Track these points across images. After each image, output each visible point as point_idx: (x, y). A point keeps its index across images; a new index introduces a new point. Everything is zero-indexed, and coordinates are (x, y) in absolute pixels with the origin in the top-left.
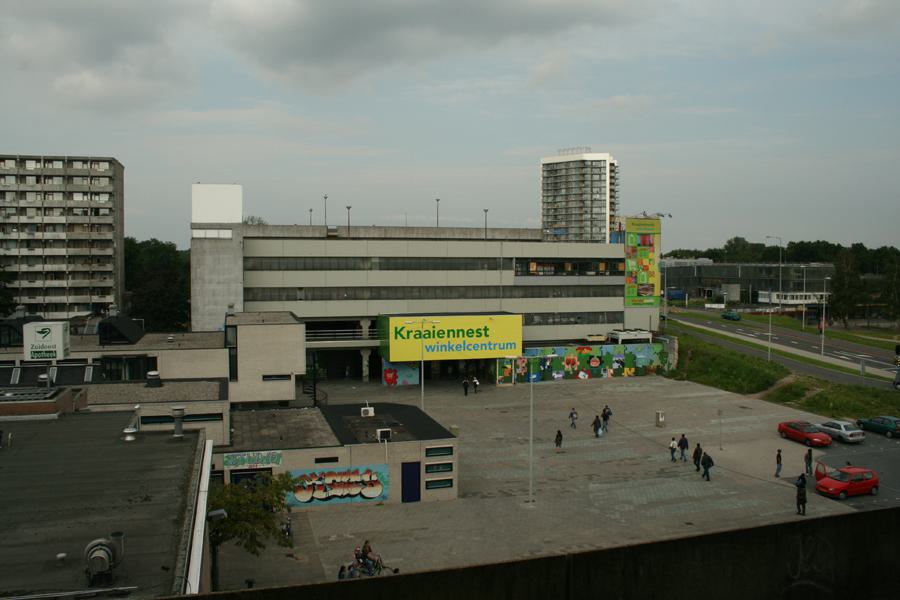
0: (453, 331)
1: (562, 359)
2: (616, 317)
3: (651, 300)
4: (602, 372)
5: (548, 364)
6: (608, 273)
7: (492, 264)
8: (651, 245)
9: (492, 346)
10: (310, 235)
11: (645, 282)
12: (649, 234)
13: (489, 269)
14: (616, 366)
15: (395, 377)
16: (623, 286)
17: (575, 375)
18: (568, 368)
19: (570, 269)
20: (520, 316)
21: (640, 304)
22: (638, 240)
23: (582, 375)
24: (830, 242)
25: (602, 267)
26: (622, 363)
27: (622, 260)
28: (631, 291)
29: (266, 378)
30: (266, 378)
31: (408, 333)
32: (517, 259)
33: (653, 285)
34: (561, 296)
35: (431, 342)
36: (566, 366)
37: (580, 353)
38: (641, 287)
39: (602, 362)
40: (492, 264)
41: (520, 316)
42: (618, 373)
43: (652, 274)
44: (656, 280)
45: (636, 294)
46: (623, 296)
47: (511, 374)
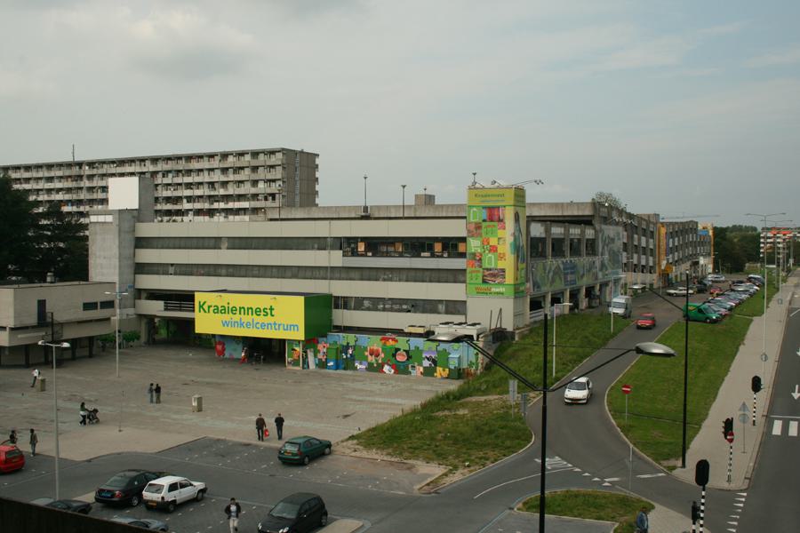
0: (244, 308)
1: (366, 349)
2: (456, 307)
3: (502, 289)
4: (410, 369)
5: (350, 352)
6: (445, 255)
7: (320, 243)
8: (500, 220)
9: (277, 327)
10: (444, 215)
11: (493, 266)
12: (498, 207)
13: (319, 249)
14: (426, 363)
15: (224, 349)
16: (465, 270)
17: (380, 368)
18: (371, 359)
19: (400, 250)
20: (303, 298)
21: (487, 293)
22: (484, 214)
23: (386, 368)
25: (438, 247)
26: (434, 362)
27: (463, 240)
28: (474, 277)
31: (209, 307)
33: (503, 271)
34: (391, 280)
35: (227, 317)
36: (370, 357)
37: (385, 344)
38: (487, 273)
39: (409, 357)
40: (320, 243)
41: (303, 298)
42: (429, 372)
43: (502, 257)
44: (508, 263)
45: (480, 280)
46: (464, 282)
47: (299, 356)
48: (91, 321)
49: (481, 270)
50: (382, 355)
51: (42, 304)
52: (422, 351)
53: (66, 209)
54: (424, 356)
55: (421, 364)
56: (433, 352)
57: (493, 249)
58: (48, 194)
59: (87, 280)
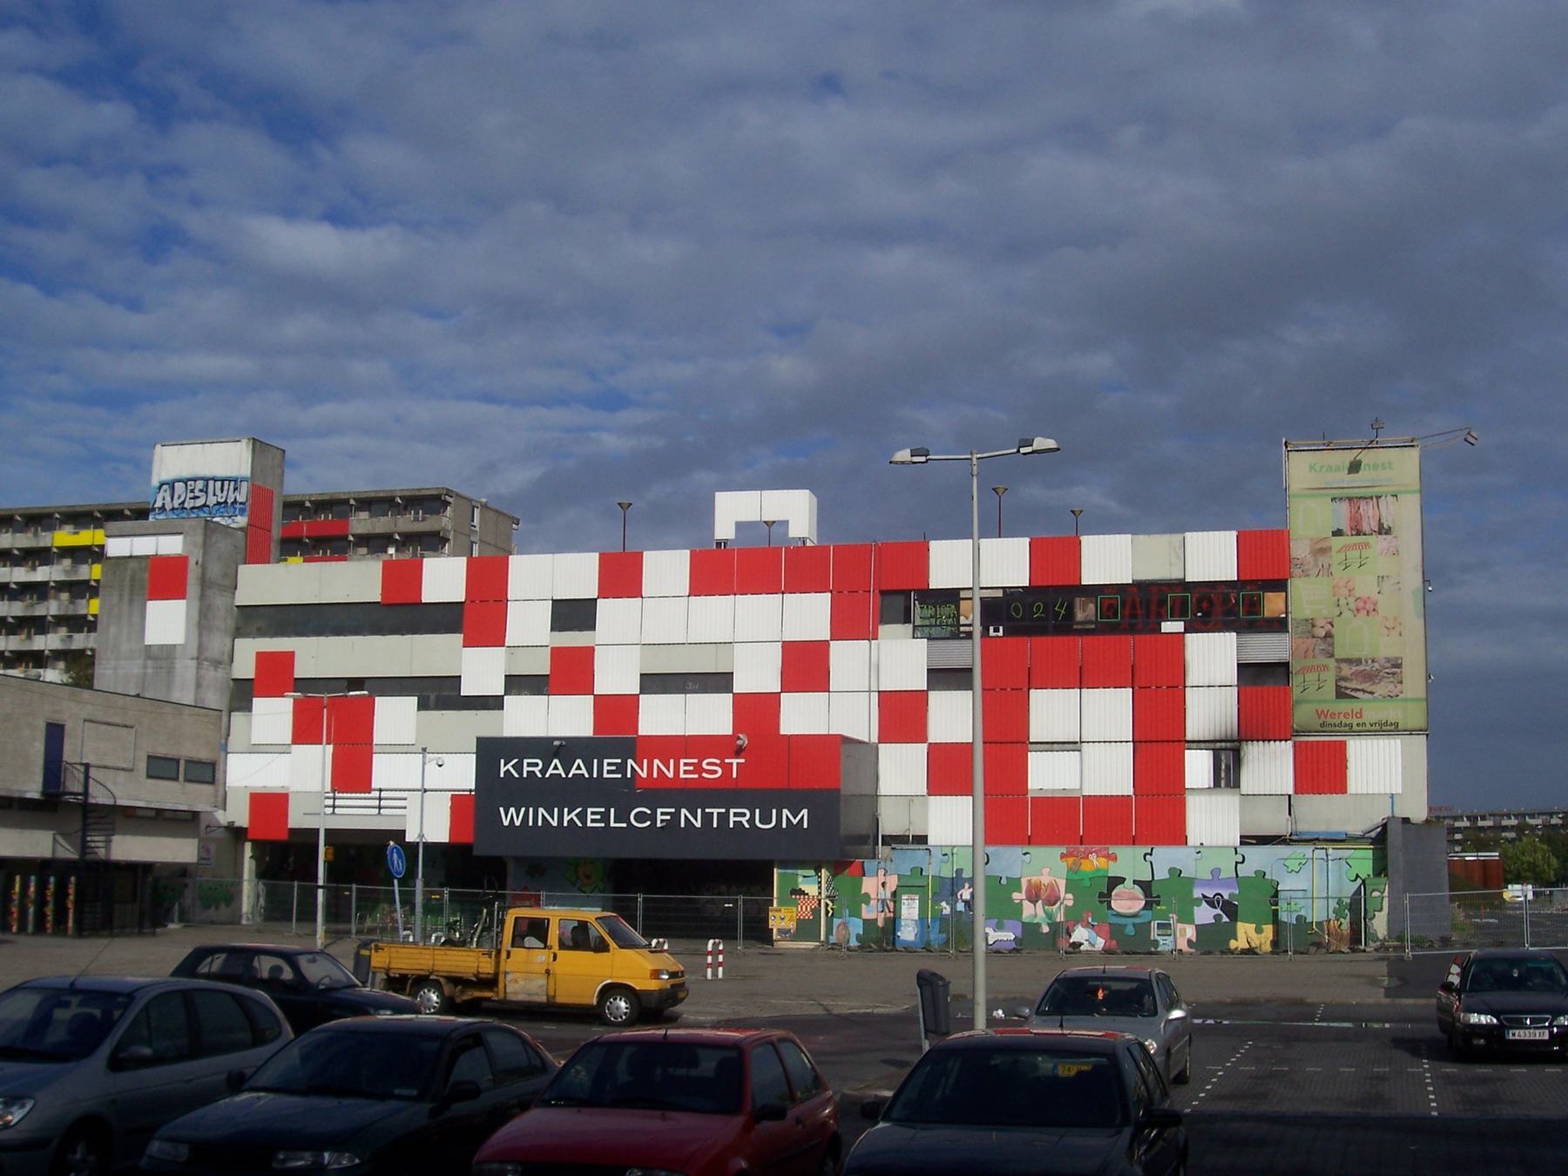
1: (1015, 884)
14: (1205, 914)
16: (1286, 665)
18: (1032, 912)
24: (450, 804)
26: (1230, 909)
29: (305, 814)
30: (305, 814)
36: (1028, 907)
45: (1330, 690)
47: (816, 912)
48: (973, 724)
49: (1332, 663)
50: (1069, 900)
51: (55, 734)
54: (1197, 893)
55: (1187, 918)
56: (1226, 883)
57: (1366, 608)
59: (464, 646)
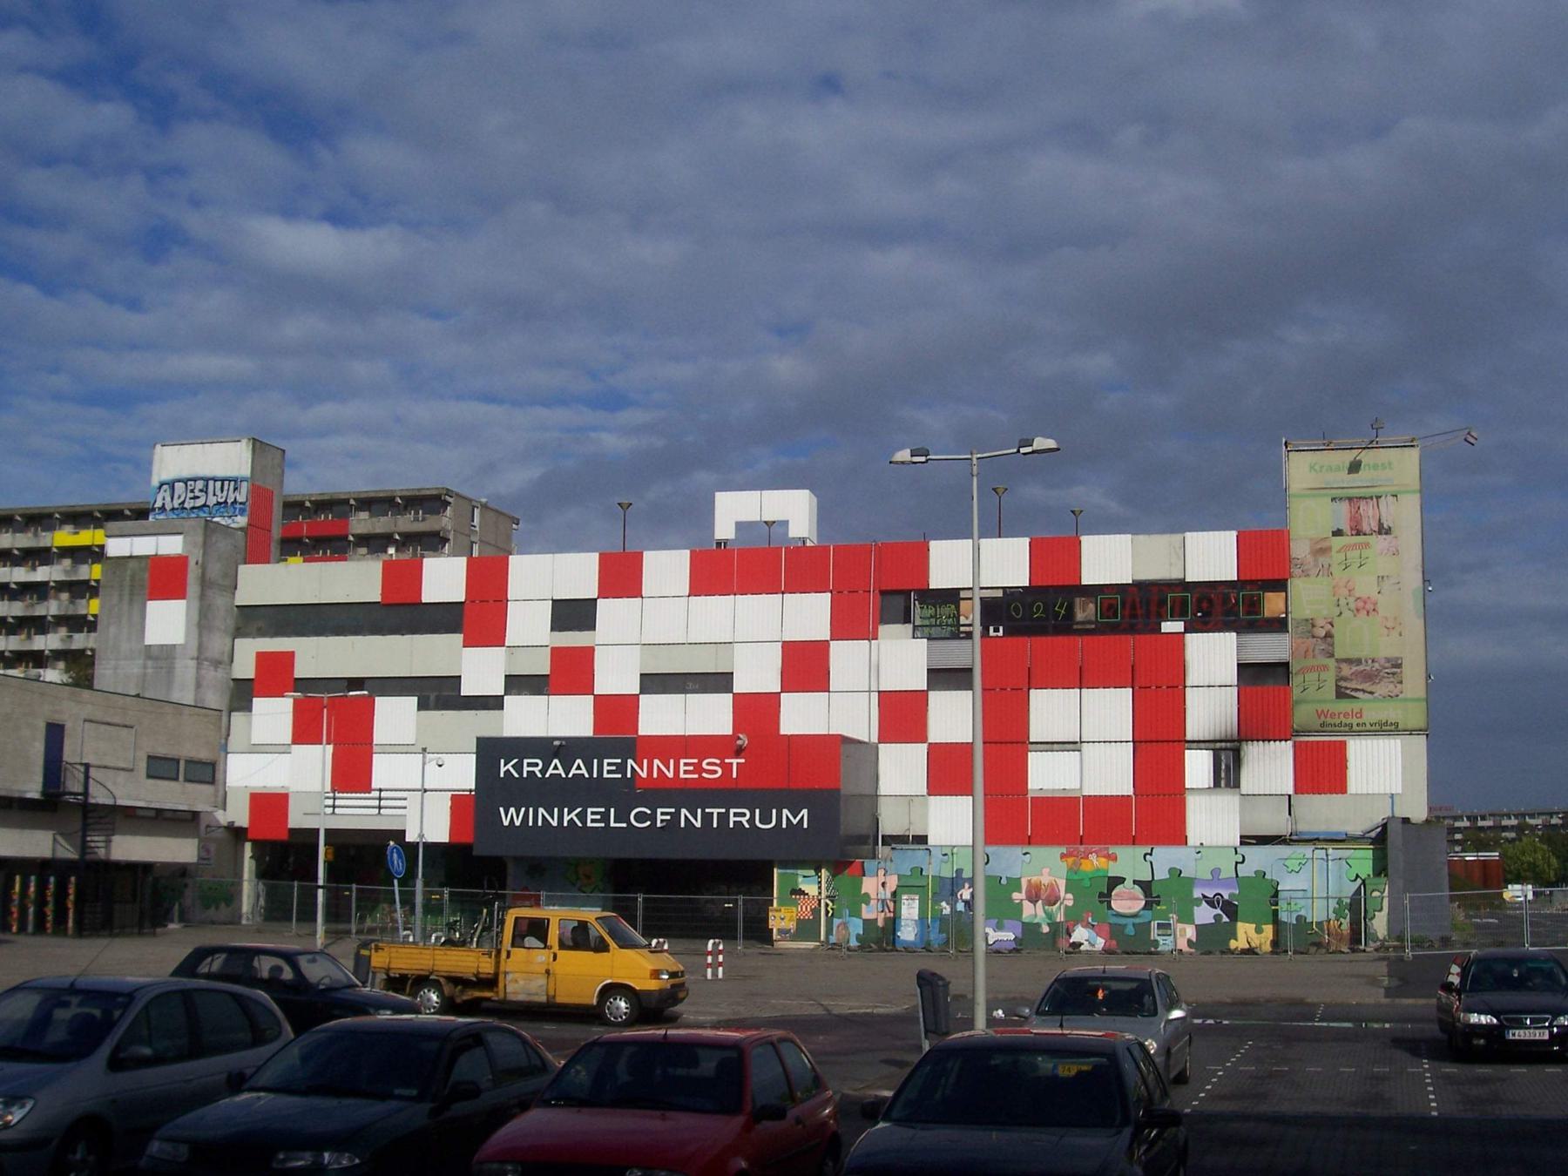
1: (1015, 884)
5: (966, 894)
14: (1205, 914)
16: (1286, 665)
18: (1032, 912)
26: (1230, 909)
29: (305, 814)
30: (305, 814)
31: (1322, 467)
32: (189, 762)
36: (1028, 906)
45: (1330, 691)
49: (1331, 663)
51: (55, 734)
52: (1192, 882)
53: (943, 1081)
54: (1197, 894)
55: (1187, 918)
56: (1225, 883)
57: (1366, 607)
58: (470, 907)
